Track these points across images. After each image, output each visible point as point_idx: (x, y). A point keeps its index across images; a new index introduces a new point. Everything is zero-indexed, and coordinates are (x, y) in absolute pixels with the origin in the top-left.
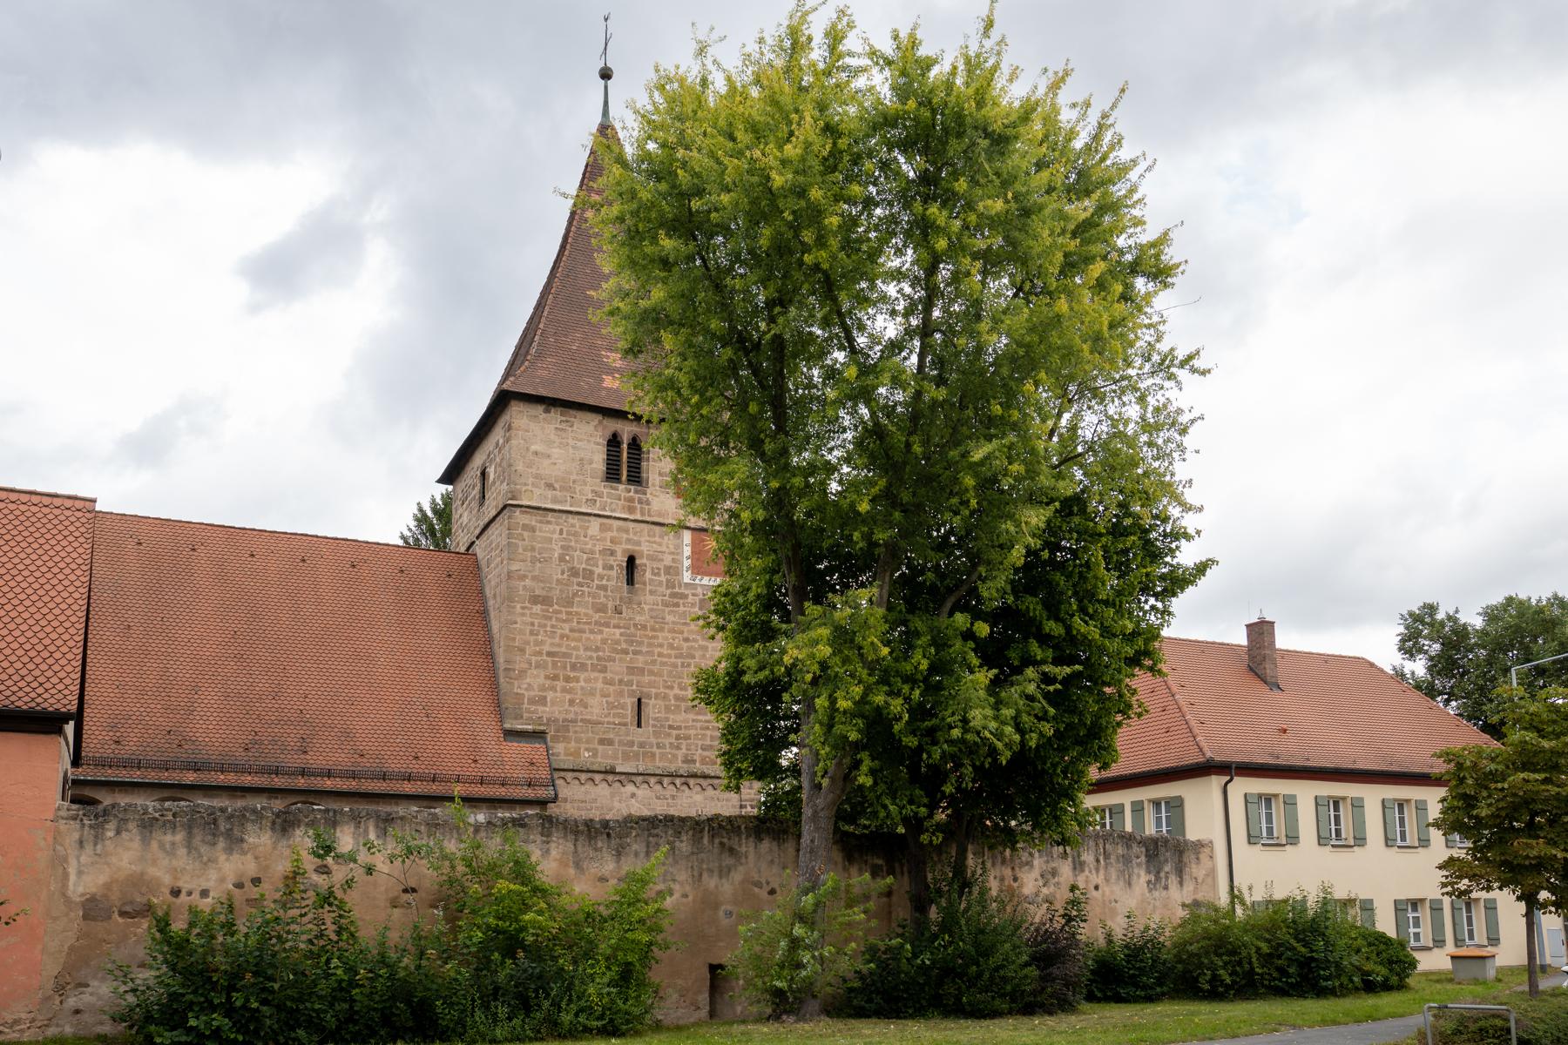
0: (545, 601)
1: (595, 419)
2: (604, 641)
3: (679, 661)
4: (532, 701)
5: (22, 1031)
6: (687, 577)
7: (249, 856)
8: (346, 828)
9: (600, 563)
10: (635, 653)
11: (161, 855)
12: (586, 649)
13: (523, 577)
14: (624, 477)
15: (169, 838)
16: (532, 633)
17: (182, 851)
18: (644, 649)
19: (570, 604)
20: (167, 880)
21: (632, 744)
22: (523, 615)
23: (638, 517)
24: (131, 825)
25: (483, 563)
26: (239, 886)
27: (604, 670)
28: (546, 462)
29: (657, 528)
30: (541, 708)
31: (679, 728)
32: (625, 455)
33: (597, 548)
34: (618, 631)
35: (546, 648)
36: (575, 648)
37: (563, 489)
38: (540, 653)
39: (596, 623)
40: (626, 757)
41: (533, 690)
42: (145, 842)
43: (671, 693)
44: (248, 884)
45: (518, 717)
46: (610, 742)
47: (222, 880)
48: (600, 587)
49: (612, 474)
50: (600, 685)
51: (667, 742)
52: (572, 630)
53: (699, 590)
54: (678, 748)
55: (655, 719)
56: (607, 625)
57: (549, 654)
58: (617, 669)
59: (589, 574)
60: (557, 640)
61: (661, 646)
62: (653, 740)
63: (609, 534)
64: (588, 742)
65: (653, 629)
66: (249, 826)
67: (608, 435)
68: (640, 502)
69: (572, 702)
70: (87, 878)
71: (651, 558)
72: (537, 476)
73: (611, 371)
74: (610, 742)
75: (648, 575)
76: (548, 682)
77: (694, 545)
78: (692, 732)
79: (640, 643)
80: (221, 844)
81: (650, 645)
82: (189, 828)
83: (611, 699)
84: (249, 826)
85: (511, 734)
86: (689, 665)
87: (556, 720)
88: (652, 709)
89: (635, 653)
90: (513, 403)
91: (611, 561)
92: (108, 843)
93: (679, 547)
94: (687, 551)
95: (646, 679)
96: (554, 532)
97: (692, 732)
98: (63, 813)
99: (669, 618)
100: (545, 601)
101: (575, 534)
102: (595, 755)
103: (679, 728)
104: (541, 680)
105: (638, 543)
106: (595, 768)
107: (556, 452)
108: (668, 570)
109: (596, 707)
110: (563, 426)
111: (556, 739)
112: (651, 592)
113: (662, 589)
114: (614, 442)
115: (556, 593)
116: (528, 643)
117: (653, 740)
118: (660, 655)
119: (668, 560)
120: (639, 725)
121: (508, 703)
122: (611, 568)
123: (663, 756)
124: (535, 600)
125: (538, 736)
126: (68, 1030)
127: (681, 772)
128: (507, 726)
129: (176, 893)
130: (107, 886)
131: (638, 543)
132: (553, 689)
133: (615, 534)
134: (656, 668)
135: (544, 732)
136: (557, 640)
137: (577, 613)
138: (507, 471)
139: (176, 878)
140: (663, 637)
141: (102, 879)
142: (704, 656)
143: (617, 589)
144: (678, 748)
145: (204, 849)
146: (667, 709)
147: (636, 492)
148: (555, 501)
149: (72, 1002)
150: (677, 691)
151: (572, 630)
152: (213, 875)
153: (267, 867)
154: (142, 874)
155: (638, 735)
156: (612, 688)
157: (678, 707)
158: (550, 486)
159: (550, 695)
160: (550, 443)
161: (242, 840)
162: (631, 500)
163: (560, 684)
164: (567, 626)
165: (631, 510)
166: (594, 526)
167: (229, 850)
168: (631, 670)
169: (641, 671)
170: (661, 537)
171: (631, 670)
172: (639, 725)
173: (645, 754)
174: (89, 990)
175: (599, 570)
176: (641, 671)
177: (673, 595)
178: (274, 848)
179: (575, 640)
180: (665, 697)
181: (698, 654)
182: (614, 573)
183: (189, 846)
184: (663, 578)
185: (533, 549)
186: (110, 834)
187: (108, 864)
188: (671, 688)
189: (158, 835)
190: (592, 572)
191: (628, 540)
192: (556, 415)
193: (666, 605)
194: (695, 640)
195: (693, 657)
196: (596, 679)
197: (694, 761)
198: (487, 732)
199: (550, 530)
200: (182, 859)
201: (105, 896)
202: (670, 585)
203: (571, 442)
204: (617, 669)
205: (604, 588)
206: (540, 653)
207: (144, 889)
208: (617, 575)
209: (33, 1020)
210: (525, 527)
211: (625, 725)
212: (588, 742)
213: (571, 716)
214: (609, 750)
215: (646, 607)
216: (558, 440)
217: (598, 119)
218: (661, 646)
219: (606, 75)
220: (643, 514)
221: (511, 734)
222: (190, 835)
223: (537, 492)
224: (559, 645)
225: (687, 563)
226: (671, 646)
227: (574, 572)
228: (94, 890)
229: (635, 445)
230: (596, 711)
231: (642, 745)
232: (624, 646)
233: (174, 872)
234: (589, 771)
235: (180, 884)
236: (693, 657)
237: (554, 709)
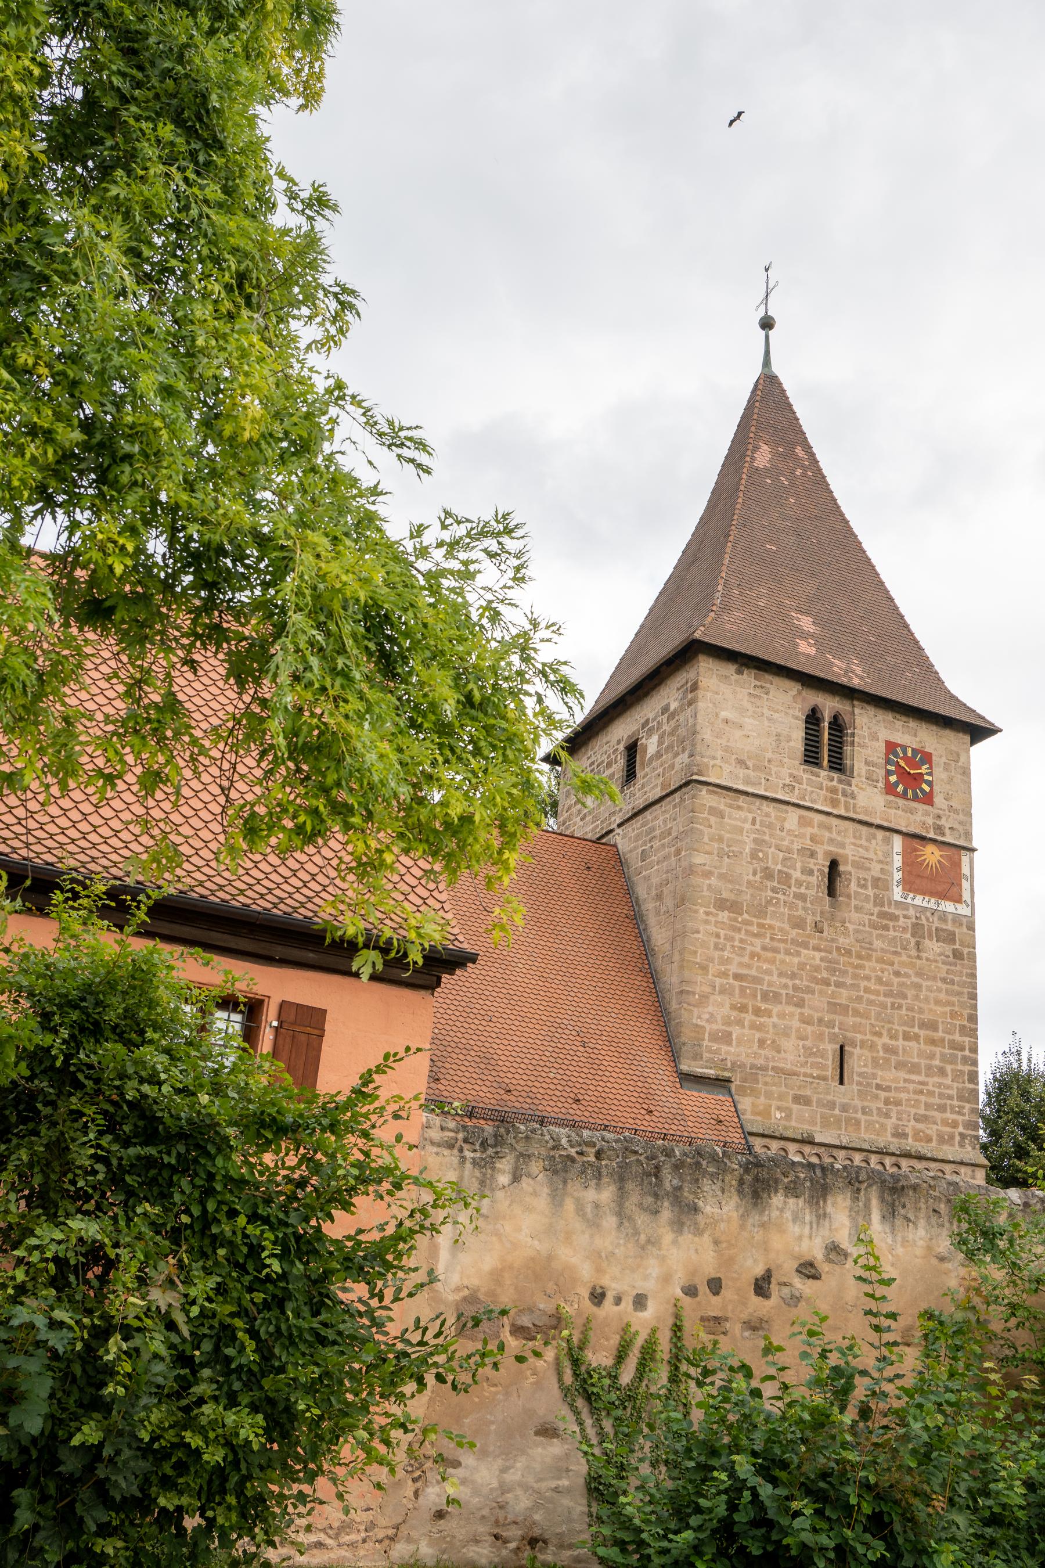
0: (734, 907)
1: (794, 688)
2: (802, 966)
3: (889, 1000)
4: (714, 1038)
5: (352, 1545)
6: (897, 893)
7: (706, 1238)
8: (840, 1199)
9: (799, 865)
10: (838, 985)
11: (578, 1225)
12: (781, 974)
13: (708, 874)
14: (825, 763)
15: (591, 1195)
16: (716, 947)
17: (610, 1221)
18: (849, 981)
19: (762, 913)
20: (586, 1272)
21: (832, 1105)
22: (707, 922)
23: (842, 812)
24: (535, 1167)
25: (634, 862)
26: (691, 1291)
27: (801, 1004)
28: (738, 733)
29: (864, 829)
30: (724, 1048)
31: (888, 1089)
32: (826, 736)
33: (796, 847)
34: (818, 955)
35: (733, 969)
36: (768, 972)
37: (756, 768)
38: (725, 974)
39: (794, 942)
40: (826, 1123)
41: (715, 1022)
42: (556, 1198)
43: (880, 1042)
44: (703, 1289)
45: (697, 1057)
46: (806, 1101)
47: (666, 1279)
48: (797, 896)
49: (811, 757)
50: (795, 1023)
51: (874, 1106)
52: (764, 948)
53: (912, 912)
54: (887, 1116)
55: (860, 1074)
56: (805, 945)
57: (737, 977)
58: (817, 1003)
59: (785, 878)
60: (746, 959)
61: (868, 978)
62: (857, 1103)
63: (809, 831)
64: (781, 1097)
65: (859, 957)
66: (706, 1184)
67: (807, 710)
68: (845, 794)
69: (762, 1043)
70: (465, 1258)
71: (856, 865)
72: (727, 749)
73: (805, 636)
74: (806, 1101)
75: (853, 886)
76: (734, 1014)
77: (906, 853)
78: (903, 1096)
79: (844, 973)
80: (667, 1213)
81: (855, 976)
82: (621, 1180)
83: (808, 1043)
84: (706, 1184)
85: (689, 1079)
86: (900, 1007)
87: (743, 1066)
88: (858, 1061)
89: (838, 985)
90: (701, 658)
91: (811, 864)
92: (500, 1195)
93: (888, 854)
94: (898, 861)
95: (851, 1020)
96: (745, 821)
97: (903, 1096)
98: (435, 1134)
99: (878, 944)
100: (734, 907)
101: (770, 826)
102: (788, 1117)
103: (888, 1089)
104: (726, 1010)
105: (842, 845)
106: (789, 1134)
107: (749, 722)
108: (876, 881)
109: (791, 1053)
110: (758, 692)
111: (742, 1090)
112: (858, 909)
113: (869, 906)
114: (813, 718)
115: (746, 898)
116: (712, 960)
117: (857, 1103)
118: (867, 990)
119: (876, 869)
120: (841, 1083)
121: (686, 1036)
122: (811, 873)
123: (869, 1124)
124: (722, 904)
125: (721, 1083)
126: (426, 1551)
127: (892, 1149)
128: (684, 1067)
129: (598, 1297)
130: (496, 1276)
131: (842, 845)
132: (740, 1023)
133: (815, 830)
134: (861, 1007)
135: (728, 1081)
136: (746, 959)
137: (771, 927)
138: (687, 740)
139: (599, 1270)
140: (871, 967)
141: (489, 1262)
142: (917, 997)
143: (816, 900)
144: (887, 1116)
145: (642, 1219)
146: (875, 1060)
147: (840, 781)
148: (747, 782)
149: (433, 1495)
150: (885, 1039)
151: (764, 948)
152: (654, 1268)
153: (731, 1260)
154: (550, 1258)
155: (841, 1094)
156: (810, 1029)
157: (887, 1060)
158: (741, 763)
159: (736, 1031)
160: (742, 711)
161: (696, 1209)
162: (834, 791)
163: (748, 1017)
164: (758, 942)
165: (834, 803)
166: (793, 817)
167: (678, 1226)
168: (834, 1007)
169: (844, 1009)
170: (868, 840)
171: (834, 1007)
172: (841, 1083)
173: (848, 1120)
174: (460, 1472)
175: (796, 874)
176: (844, 1009)
177: (882, 915)
178: (742, 1227)
179: (766, 961)
180: (872, 1047)
181: (911, 993)
182: (813, 880)
183: (620, 1213)
184: (870, 892)
185: (720, 839)
186: (504, 1179)
187: (497, 1234)
188: (879, 1034)
189: (574, 1187)
190: (788, 876)
191: (831, 841)
192: (749, 677)
193: (874, 926)
194: (907, 975)
195: (905, 997)
196: (792, 1015)
197: (905, 1135)
198: (662, 1076)
199: (741, 817)
200: (609, 1236)
201: (492, 1293)
202: (879, 901)
203: (765, 711)
204: (817, 1003)
205: (802, 897)
206: (725, 974)
207: (551, 1287)
208: (817, 881)
209: (371, 1526)
210: (713, 811)
211: (825, 1079)
212: (781, 1097)
213: (760, 1062)
214: (806, 1112)
215: (851, 927)
216: (749, 706)
217: (755, 372)
218: (868, 978)
219: (767, 324)
220: (847, 809)
221: (689, 1079)
222: (622, 1194)
223: (727, 768)
224: (749, 966)
225: (898, 876)
226: (879, 980)
227: (768, 874)
228: (474, 1282)
229: (837, 726)
230: (791, 1057)
231: (844, 1108)
232: (825, 974)
233: (598, 1258)
234: (763, 1136)
235: (605, 1281)
236: (905, 997)
237: (738, 1051)
